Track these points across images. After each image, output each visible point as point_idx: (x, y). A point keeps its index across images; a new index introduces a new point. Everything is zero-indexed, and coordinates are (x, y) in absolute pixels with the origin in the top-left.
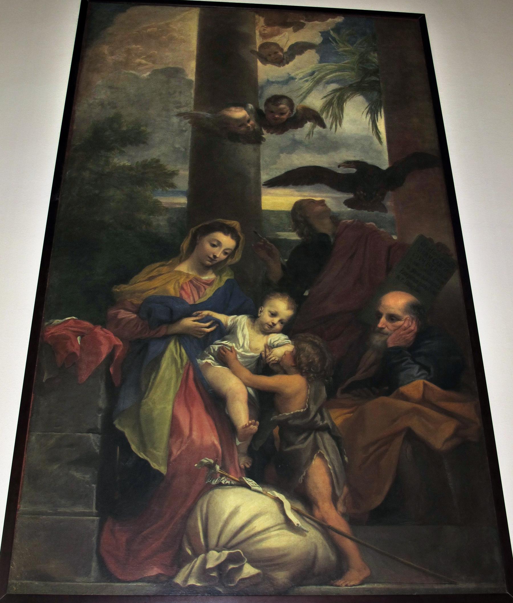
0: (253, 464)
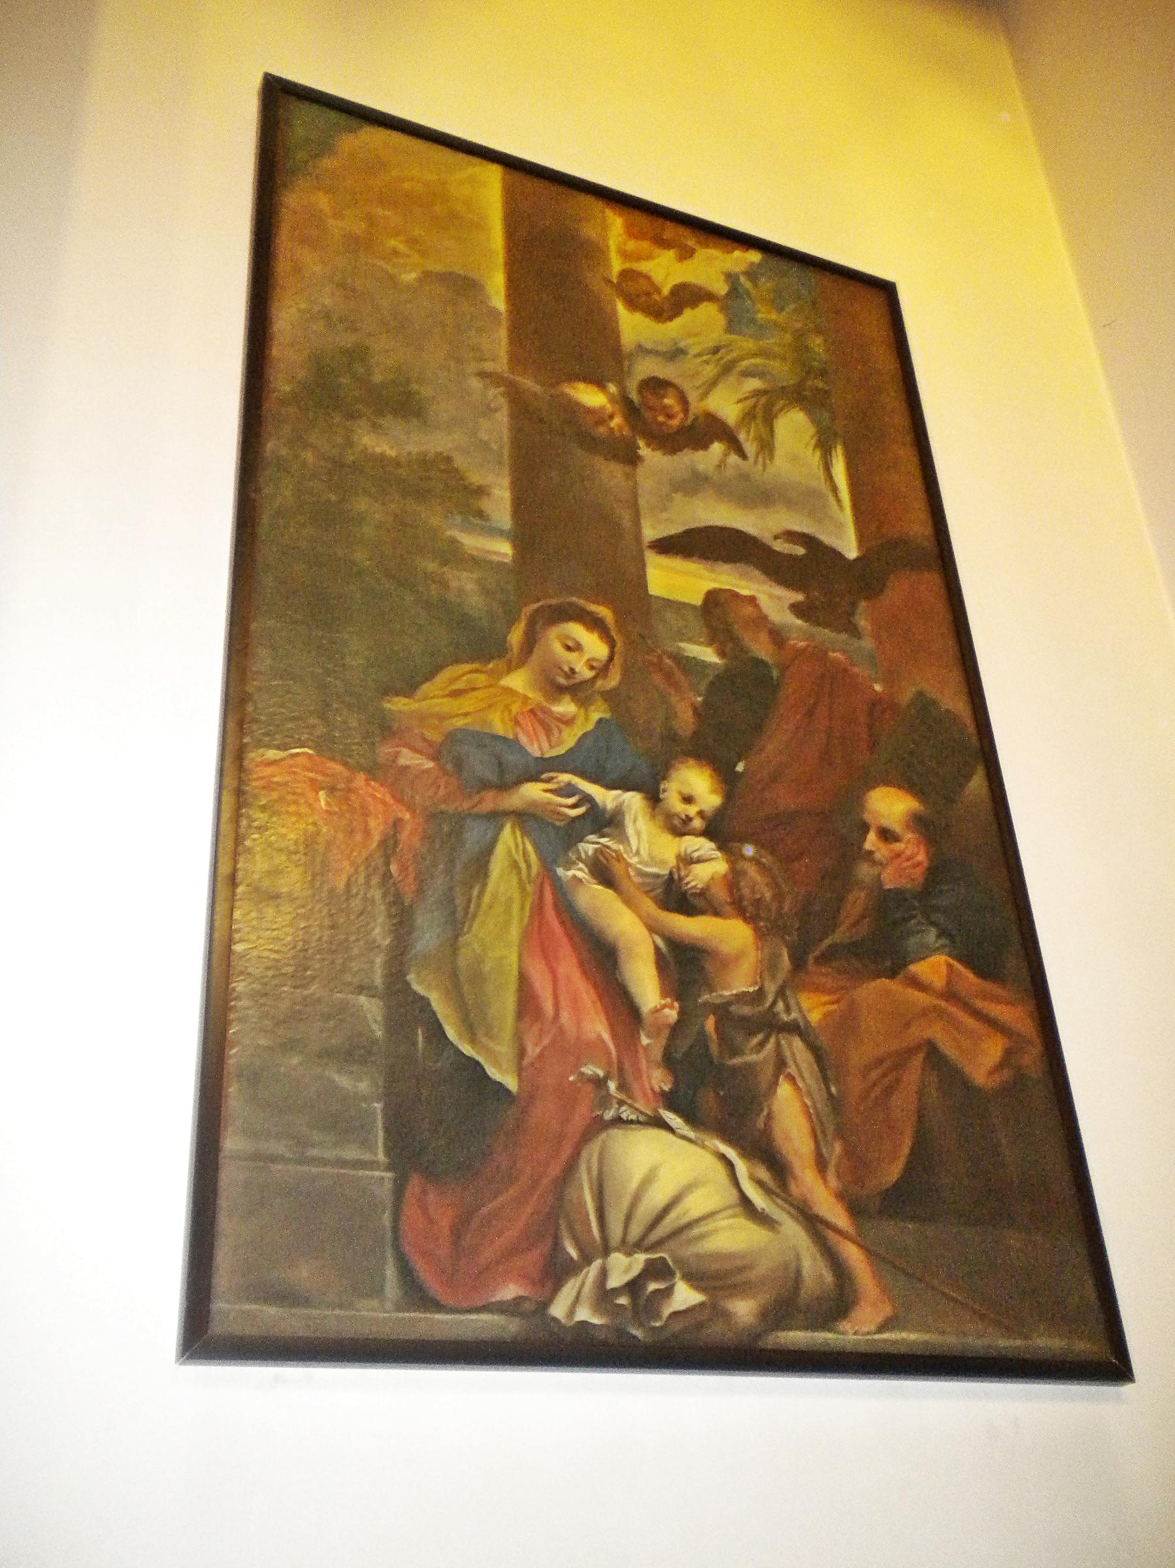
0: (676, 1083)
